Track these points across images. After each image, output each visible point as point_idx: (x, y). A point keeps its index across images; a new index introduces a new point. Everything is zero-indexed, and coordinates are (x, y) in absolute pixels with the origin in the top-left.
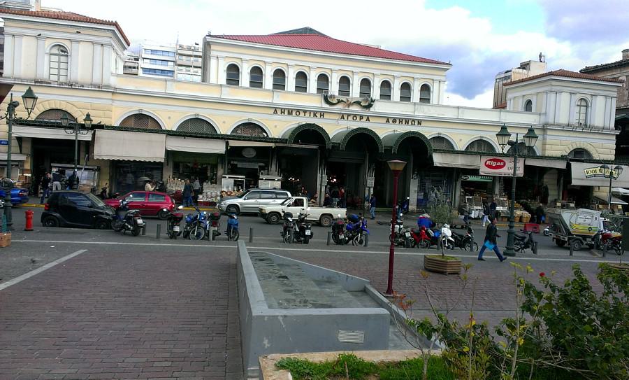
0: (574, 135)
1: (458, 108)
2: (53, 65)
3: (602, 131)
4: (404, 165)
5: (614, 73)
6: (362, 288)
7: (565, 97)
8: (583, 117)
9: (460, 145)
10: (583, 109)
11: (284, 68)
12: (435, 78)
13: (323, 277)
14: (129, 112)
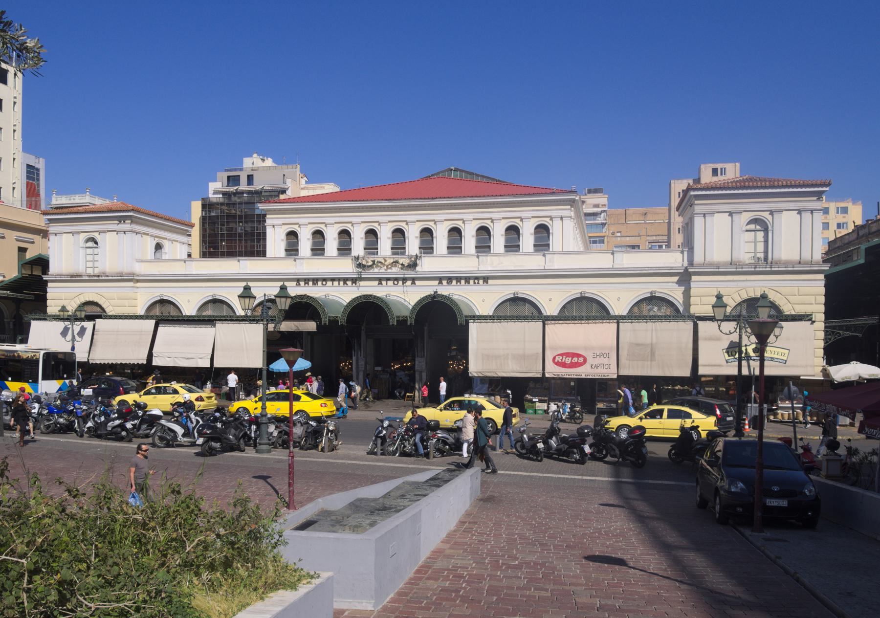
8: (761, 247)
12: (553, 214)
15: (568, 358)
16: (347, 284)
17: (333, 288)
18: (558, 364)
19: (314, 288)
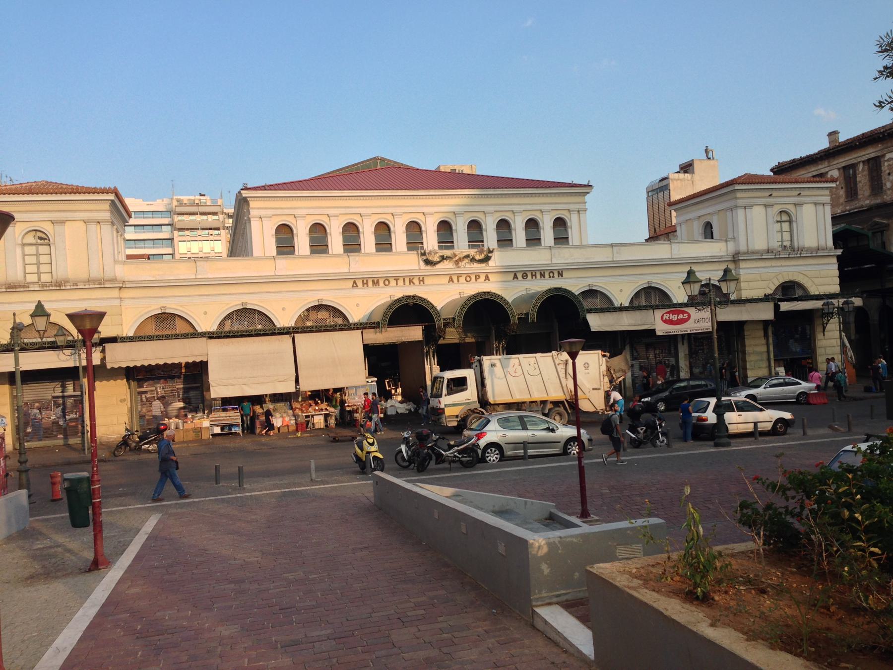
0: (779, 263)
1: (612, 245)
2: (28, 260)
3: (816, 253)
4: (583, 344)
5: (820, 167)
6: (546, 515)
7: (758, 213)
8: (787, 236)
9: (622, 298)
10: (786, 226)
11: (356, 220)
12: (571, 207)
13: (494, 506)
14: (146, 313)
15: (674, 316)
16: (414, 284)
17: (398, 288)
18: (666, 322)
19: (542, 281)
